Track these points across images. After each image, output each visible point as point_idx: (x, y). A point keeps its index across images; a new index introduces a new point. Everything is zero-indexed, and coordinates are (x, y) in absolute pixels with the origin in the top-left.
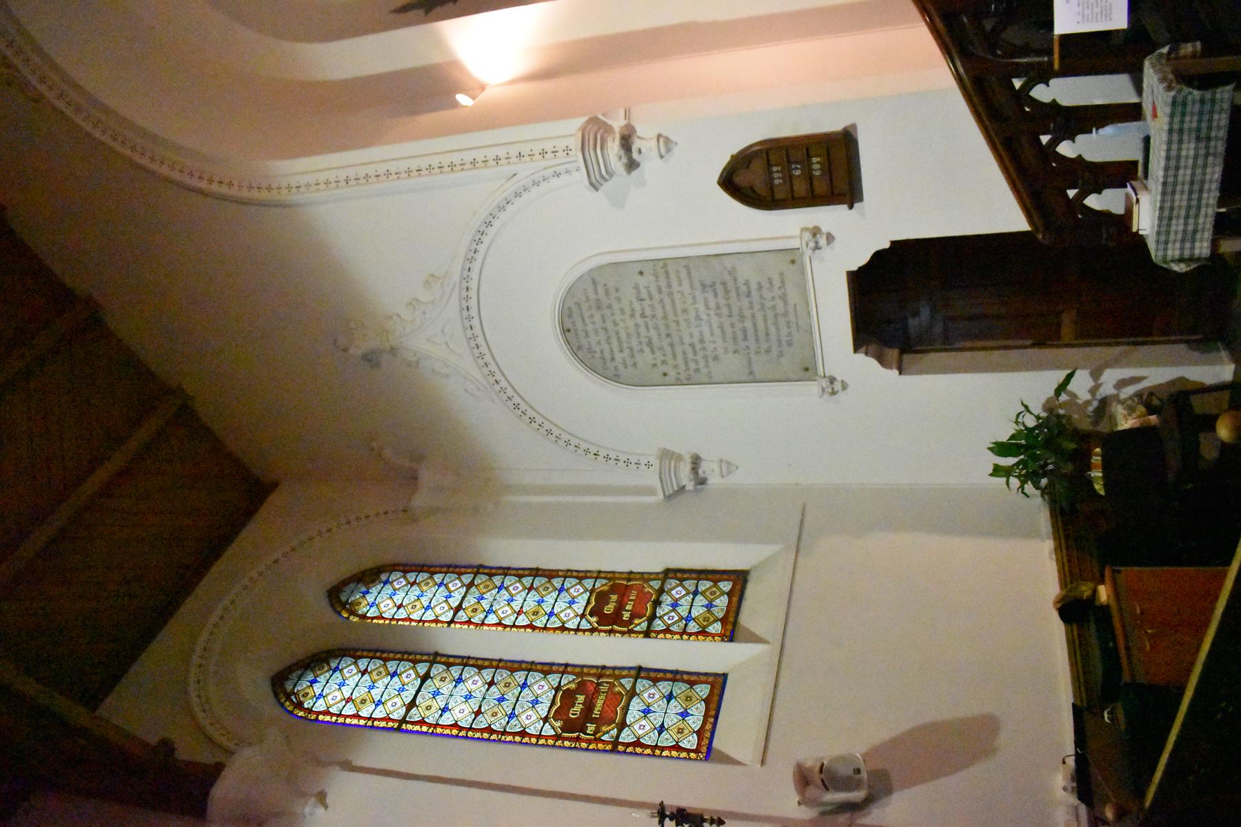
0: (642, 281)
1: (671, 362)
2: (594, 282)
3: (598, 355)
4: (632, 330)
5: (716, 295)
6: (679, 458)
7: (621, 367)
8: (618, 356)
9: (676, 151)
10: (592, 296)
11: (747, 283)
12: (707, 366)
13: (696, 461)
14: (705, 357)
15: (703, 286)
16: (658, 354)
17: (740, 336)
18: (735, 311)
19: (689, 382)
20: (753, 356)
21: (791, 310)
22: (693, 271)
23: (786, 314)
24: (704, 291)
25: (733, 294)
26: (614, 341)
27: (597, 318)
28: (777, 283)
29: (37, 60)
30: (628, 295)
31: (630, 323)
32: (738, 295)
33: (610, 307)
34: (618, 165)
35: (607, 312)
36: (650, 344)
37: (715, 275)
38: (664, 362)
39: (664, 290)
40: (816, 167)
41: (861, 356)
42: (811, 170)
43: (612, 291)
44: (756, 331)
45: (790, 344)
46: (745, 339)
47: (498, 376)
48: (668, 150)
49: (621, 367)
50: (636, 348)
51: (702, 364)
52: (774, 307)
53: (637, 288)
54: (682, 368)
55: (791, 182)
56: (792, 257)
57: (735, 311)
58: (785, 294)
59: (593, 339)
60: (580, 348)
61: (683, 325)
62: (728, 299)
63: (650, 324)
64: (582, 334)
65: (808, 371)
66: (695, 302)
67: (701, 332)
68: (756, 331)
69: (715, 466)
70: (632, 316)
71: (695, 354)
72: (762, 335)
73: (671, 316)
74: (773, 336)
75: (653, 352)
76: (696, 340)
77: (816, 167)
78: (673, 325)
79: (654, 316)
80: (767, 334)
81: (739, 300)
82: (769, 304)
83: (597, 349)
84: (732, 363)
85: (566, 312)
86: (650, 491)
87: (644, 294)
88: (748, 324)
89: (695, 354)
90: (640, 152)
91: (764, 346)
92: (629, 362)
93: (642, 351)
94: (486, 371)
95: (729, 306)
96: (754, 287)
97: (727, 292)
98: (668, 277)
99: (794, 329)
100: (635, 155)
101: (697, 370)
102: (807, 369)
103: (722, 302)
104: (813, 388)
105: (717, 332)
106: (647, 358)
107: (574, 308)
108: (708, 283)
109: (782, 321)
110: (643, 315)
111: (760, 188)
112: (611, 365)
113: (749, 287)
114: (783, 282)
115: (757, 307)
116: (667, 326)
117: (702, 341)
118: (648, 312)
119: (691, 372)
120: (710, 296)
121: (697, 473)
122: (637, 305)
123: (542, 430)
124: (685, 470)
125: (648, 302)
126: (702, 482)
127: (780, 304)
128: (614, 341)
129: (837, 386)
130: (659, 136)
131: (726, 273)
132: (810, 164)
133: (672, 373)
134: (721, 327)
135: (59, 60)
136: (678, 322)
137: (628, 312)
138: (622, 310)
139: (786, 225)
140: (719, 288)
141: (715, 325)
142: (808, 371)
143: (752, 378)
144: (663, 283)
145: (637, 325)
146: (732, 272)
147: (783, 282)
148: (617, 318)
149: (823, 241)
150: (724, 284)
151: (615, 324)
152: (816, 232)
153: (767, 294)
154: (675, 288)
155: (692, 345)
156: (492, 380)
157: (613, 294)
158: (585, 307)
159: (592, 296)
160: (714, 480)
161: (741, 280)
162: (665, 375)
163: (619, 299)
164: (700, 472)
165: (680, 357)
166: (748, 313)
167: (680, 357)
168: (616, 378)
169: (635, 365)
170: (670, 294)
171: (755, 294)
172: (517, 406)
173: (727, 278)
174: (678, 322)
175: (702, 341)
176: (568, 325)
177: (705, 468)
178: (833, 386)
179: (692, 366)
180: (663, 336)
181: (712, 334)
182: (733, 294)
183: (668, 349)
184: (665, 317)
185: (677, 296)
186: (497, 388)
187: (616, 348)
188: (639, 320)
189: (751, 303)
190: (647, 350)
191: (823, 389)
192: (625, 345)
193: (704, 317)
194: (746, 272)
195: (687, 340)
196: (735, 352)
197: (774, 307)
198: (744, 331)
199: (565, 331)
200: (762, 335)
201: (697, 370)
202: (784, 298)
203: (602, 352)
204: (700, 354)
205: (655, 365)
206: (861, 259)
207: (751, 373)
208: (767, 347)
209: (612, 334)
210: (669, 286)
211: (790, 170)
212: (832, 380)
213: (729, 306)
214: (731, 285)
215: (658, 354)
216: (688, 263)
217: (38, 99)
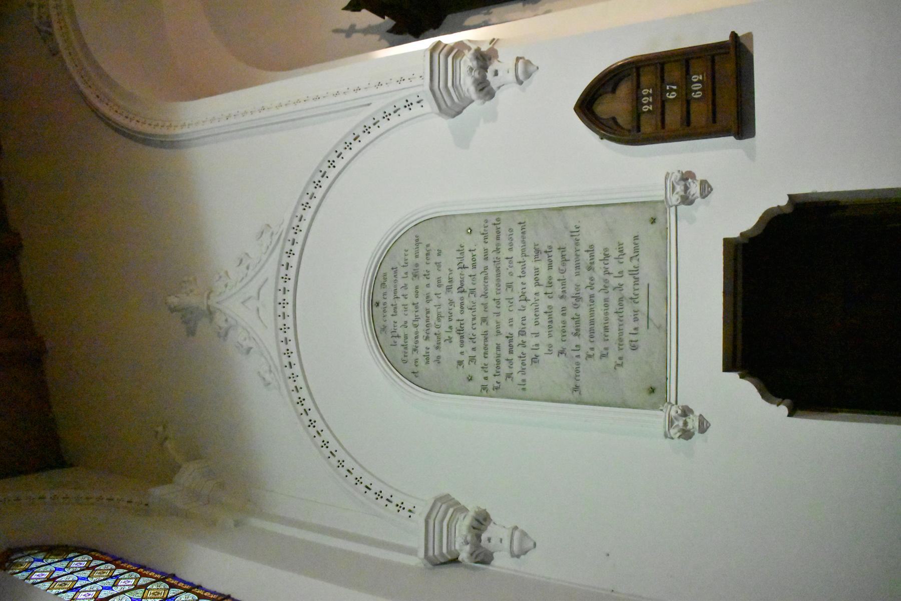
0: (469, 242)
1: (480, 360)
2: (417, 241)
3: (400, 341)
4: (444, 310)
5: (550, 267)
6: (464, 510)
7: (422, 362)
8: (423, 345)
9: (535, 77)
10: (411, 258)
11: (591, 250)
12: (523, 371)
13: (481, 521)
14: (522, 356)
15: (538, 251)
16: (468, 346)
17: (571, 327)
18: (571, 290)
19: (497, 391)
20: (582, 360)
21: (642, 293)
22: (527, 229)
23: (634, 300)
24: (537, 259)
25: (571, 266)
26: (422, 323)
27: (411, 291)
28: (629, 250)
29: (68, 20)
30: (450, 259)
31: (445, 298)
32: (578, 267)
33: (427, 276)
34: (467, 83)
35: (423, 281)
36: (460, 331)
37: (550, 235)
38: (472, 359)
39: (492, 256)
40: (697, 87)
41: (734, 376)
42: (689, 91)
43: (434, 253)
44: (592, 322)
45: (634, 348)
46: (577, 334)
47: (294, 359)
48: (528, 75)
49: (422, 362)
50: (445, 336)
51: (517, 366)
52: (620, 287)
53: (461, 250)
54: (492, 370)
55: (663, 106)
56: (653, 214)
57: (571, 290)
58: (637, 269)
59: (400, 318)
60: (384, 329)
61: (504, 304)
62: (562, 272)
63: (467, 303)
64: (390, 311)
65: (655, 393)
66: (523, 274)
67: (524, 319)
68: (592, 322)
69: (505, 535)
70: (449, 289)
71: (511, 352)
72: (599, 328)
73: (492, 294)
74: (614, 333)
75: (462, 344)
76: (515, 331)
77: (697, 87)
78: (492, 304)
79: (473, 291)
80: (606, 329)
81: (578, 274)
82: (614, 282)
83: (401, 331)
84: (553, 370)
85: (380, 279)
86: (412, 552)
87: (468, 262)
88: (584, 311)
89: (511, 352)
90: (496, 73)
91: (600, 346)
92: (433, 353)
93: (450, 340)
94: (283, 347)
95: (563, 282)
96: (599, 255)
97: (564, 260)
98: (498, 238)
99: (643, 321)
100: (489, 75)
101: (509, 376)
102: (652, 390)
103: (556, 275)
104: (656, 420)
105: (544, 319)
106: (451, 351)
107: (390, 275)
108: (544, 248)
109: (628, 311)
110: (461, 290)
111: (624, 120)
112: (411, 357)
113: (592, 257)
114: (636, 250)
115: (598, 286)
116: (485, 306)
117: (522, 333)
118: (468, 285)
119: (502, 379)
120: (543, 265)
121: (479, 537)
122: (456, 276)
123: (319, 440)
124: (463, 525)
125: (470, 271)
126: (483, 558)
127: (628, 281)
128: (422, 323)
129: (693, 423)
130: (518, 59)
131: (567, 235)
132: (689, 82)
133: (479, 376)
134: (549, 313)
135: (106, 67)
136: (497, 301)
137: (445, 282)
138: (439, 280)
139: (649, 168)
140: (556, 256)
141: (543, 308)
142: (655, 393)
143: (576, 395)
144: (491, 247)
145: (451, 302)
146: (574, 234)
147: (636, 250)
148: (433, 289)
149: (695, 189)
150: (562, 249)
151: (428, 299)
152: (687, 177)
153: (614, 267)
154: (505, 253)
155: (510, 337)
156: (286, 361)
157: (434, 258)
158: (401, 272)
159: (411, 258)
160: (502, 561)
161: (583, 247)
162: (470, 379)
163: (438, 264)
164: (484, 537)
165: (492, 351)
166: (585, 294)
167: (492, 351)
168: (414, 378)
169: (438, 360)
170: (497, 261)
171: (598, 265)
172: (301, 401)
173: (569, 243)
174: (497, 301)
175: (522, 333)
176: (378, 297)
177: (494, 534)
178: (687, 426)
179: (504, 366)
180: (478, 320)
181: (537, 324)
182: (571, 266)
183: (480, 343)
184: (485, 295)
185: (504, 264)
186: (288, 372)
187: (422, 334)
188: (455, 296)
189: (592, 279)
190: (456, 339)
191: (671, 423)
192: (433, 330)
193: (530, 296)
194: (593, 234)
195: (505, 329)
196: (562, 352)
197: (620, 287)
198: (577, 319)
199: (374, 304)
200: (599, 328)
201: (509, 376)
202: (635, 273)
203: (406, 337)
204: (517, 351)
205: (460, 363)
206: (744, 220)
207: (576, 388)
208: (610, 360)
209: (422, 313)
210: (498, 250)
211: (663, 91)
212: (686, 412)
213: (563, 282)
214: (570, 252)
215: (468, 346)
216: (524, 219)
217: (55, 52)
